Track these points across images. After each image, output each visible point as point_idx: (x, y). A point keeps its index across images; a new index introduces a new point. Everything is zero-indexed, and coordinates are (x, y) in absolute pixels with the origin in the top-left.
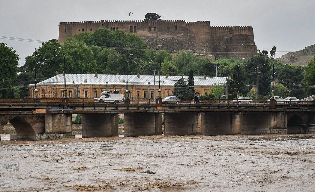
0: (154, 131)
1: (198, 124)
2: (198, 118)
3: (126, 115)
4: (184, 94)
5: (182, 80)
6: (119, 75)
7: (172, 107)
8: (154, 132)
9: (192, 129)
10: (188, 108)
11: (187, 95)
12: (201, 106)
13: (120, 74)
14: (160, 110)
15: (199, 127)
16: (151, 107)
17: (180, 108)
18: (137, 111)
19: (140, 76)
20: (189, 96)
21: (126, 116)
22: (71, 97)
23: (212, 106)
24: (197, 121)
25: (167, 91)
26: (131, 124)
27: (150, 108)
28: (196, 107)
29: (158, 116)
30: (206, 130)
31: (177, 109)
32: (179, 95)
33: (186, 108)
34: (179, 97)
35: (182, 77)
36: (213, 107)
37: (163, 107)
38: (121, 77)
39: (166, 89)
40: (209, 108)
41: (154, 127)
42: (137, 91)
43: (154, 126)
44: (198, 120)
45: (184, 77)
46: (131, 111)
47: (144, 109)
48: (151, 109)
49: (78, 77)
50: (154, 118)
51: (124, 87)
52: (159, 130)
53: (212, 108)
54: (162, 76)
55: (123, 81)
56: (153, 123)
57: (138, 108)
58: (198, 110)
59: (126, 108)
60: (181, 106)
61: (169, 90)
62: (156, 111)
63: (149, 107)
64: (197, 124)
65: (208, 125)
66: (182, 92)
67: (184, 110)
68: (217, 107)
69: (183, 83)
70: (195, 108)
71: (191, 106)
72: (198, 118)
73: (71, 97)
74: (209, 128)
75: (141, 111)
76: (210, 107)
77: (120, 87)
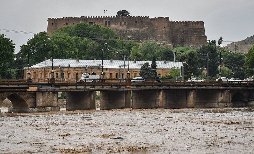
0: (124, 105)
1: (160, 100)
2: (160, 95)
3: (102, 92)
4: (148, 76)
5: (147, 64)
6: (96, 60)
7: (138, 86)
8: (124, 106)
9: (155, 104)
10: (152, 86)
11: (150, 77)
12: (162, 85)
13: (97, 60)
14: (129, 89)
15: (160, 102)
16: (121, 86)
17: (145, 87)
18: (111, 89)
19: (113, 61)
20: (152, 77)
21: (102, 93)
22: (57, 78)
23: (171, 85)
24: (159, 97)
25: (134, 73)
26: (106, 99)
27: (121, 87)
28: (158, 86)
29: (127, 93)
30: (166, 105)
31: (142, 87)
32: (145, 76)
33: (150, 87)
34: (145, 78)
35: (147, 62)
36: (171, 86)
37: (131, 86)
38: (98, 62)
39: (134, 72)
40: (169, 87)
41: (124, 102)
42: (110, 73)
43: (125, 101)
44: (160, 96)
45: (148, 62)
46: (105, 89)
47: (116, 87)
48: (122, 87)
49: (63, 62)
50: (124, 94)
51: (100, 70)
52: (128, 105)
53: (171, 86)
54: (130, 61)
55: (100, 65)
56: (123, 99)
57: (112, 86)
58: (160, 88)
59: (101, 87)
60: (146, 85)
61: (136, 72)
62: (126, 89)
63: (120, 86)
64: (159, 99)
65: (168, 100)
66: (146, 74)
67: (148, 88)
68: (175, 86)
69: (148, 67)
70: (157, 86)
71: (154, 85)
72: (159, 95)
73: (57, 78)
74: (169, 103)
75: (114, 89)
76: (170, 86)
77: (97, 70)
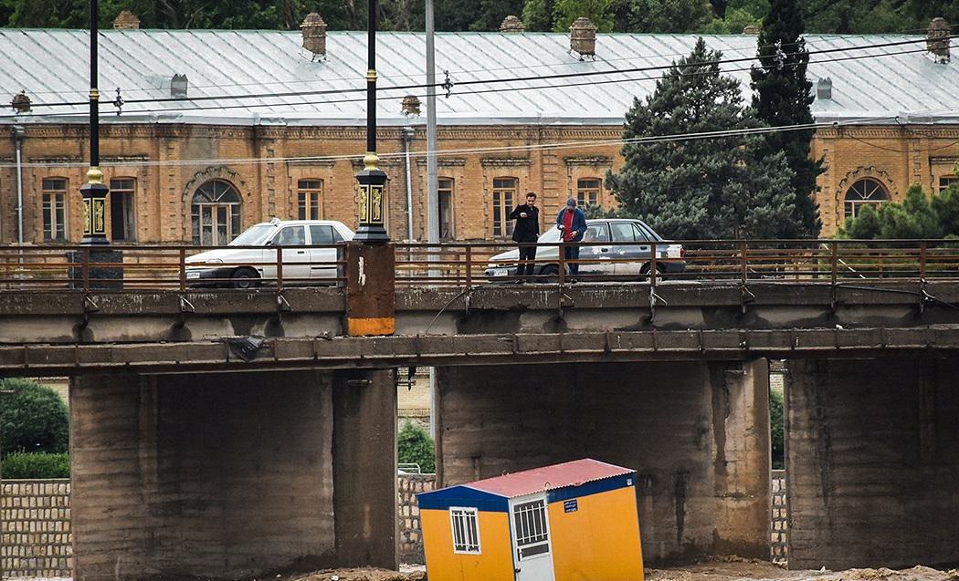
0: (321, 531)
1: (730, 468)
2: (728, 412)
3: (85, 393)
4: (715, 203)
5: (698, 71)
6: (140, 36)
7: (483, 312)
8: (329, 538)
9: (681, 513)
10: (632, 320)
11: (740, 214)
12: (752, 307)
13: (144, 25)
14: (380, 345)
15: (737, 496)
16: (293, 316)
17: (557, 323)
18: (168, 355)
19: (604, 42)
20: (760, 217)
21: (88, 405)
22: (60, 235)
23: (856, 298)
24: (721, 438)
25: (579, 172)
26: (130, 467)
27: (284, 324)
28: (705, 309)
29: (359, 391)
30: (819, 525)
31: (531, 330)
32: (672, 213)
33: (610, 324)
34: (674, 226)
35: (701, 46)
36: (861, 314)
37: (404, 319)
38: (158, 52)
39: (568, 161)
40: (830, 319)
41: (323, 500)
42: (296, 173)
43: (328, 491)
44: (729, 430)
45: (712, 43)
46: (108, 355)
47: (228, 332)
48: (298, 333)
49: (209, 56)
50: (327, 411)
51: (176, 145)
52: (367, 527)
53: (856, 316)
54: (109, 34)
55: (174, 91)
56: (313, 459)
57: (180, 322)
58: (727, 340)
59: (65, 330)
60: (569, 309)
61: (596, 165)
62: (342, 351)
63: (275, 320)
64: (721, 462)
65: (838, 474)
66: (695, 181)
67: (591, 340)
68: (900, 314)
69: (708, 100)
70: (697, 318)
71: (659, 307)
72: (724, 409)
73: (60, 235)
74: (853, 503)
75: (203, 352)
76: (841, 314)
77: (143, 145)
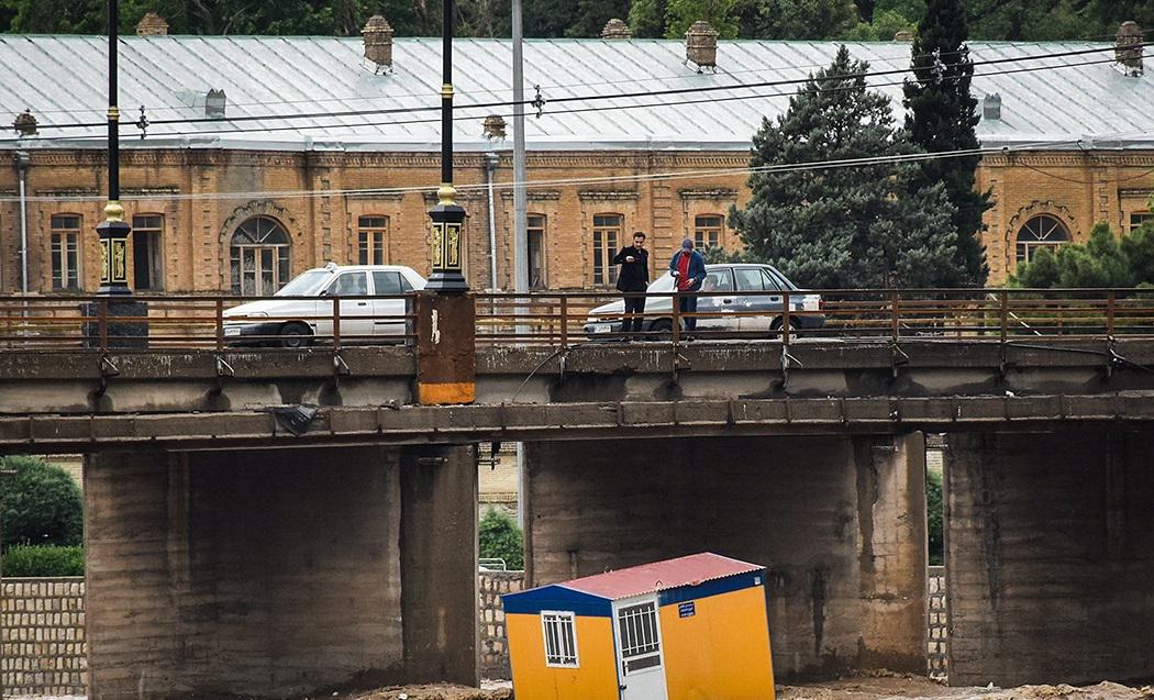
0: (386, 639)
1: (879, 564)
2: (876, 496)
3: (102, 474)
4: (860, 244)
5: (840, 85)
6: (168, 43)
7: (581, 375)
8: (396, 649)
9: (819, 618)
10: (761, 385)
11: (891, 258)
12: (905, 370)
13: (174, 31)
14: (457, 416)
15: (887, 598)
16: (352, 381)
17: (671, 389)
18: (202, 427)
19: (727, 51)
20: (915, 262)
21: (106, 488)
22: (72, 283)
23: (1030, 358)
24: (867, 528)
25: (696, 208)
26: (157, 563)
27: (342, 391)
28: (848, 373)
29: (432, 471)
30: (986, 632)
31: (639, 397)
32: (809, 257)
33: (734, 390)
34: (811, 273)
35: (843, 55)
36: (1036, 378)
37: (486, 385)
38: (190, 62)
39: (684, 194)
40: (999, 384)
41: (388, 603)
42: (357, 209)
43: (394, 592)
44: (877, 518)
45: (857, 52)
46: (130, 427)
47: (275, 400)
48: (359, 401)
49: (252, 67)
50: (394, 496)
51: (211, 175)
52: (442, 635)
53: (1030, 380)
54: (131, 41)
55: (209, 110)
56: (377, 553)
57: (216, 389)
58: (875, 410)
59: (79, 398)
60: (684, 372)
61: (717, 199)
62: (412, 422)
63: (331, 386)
64: (868, 557)
65: (1008, 571)
66: (836, 218)
67: (711, 410)
68: (1083, 379)
69: (852, 121)
70: (839, 383)
71: (793, 370)
72: (871, 493)
73: (72, 283)
74: (1027, 606)
75: (244, 424)
76: (1011, 378)
77: (172, 174)
